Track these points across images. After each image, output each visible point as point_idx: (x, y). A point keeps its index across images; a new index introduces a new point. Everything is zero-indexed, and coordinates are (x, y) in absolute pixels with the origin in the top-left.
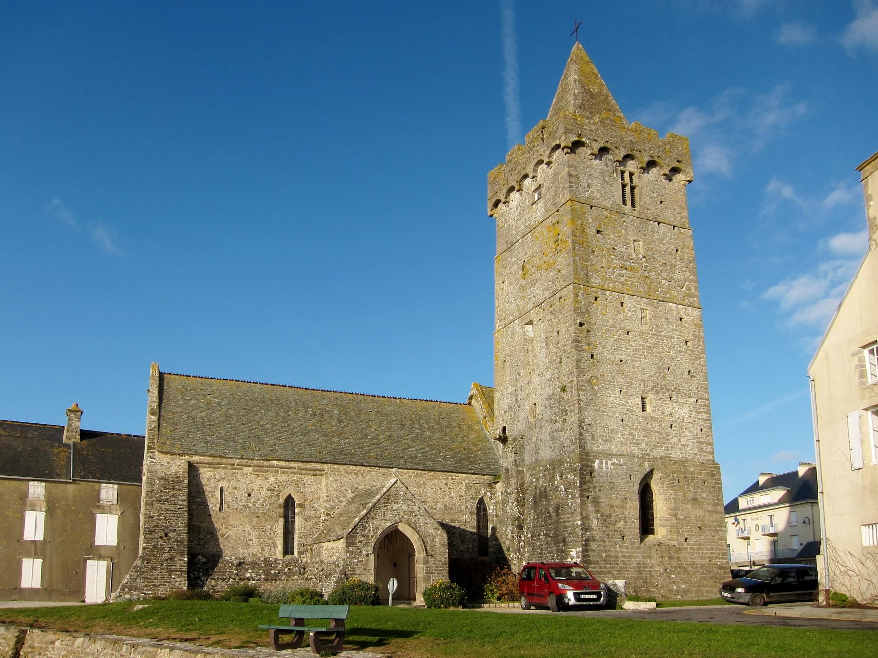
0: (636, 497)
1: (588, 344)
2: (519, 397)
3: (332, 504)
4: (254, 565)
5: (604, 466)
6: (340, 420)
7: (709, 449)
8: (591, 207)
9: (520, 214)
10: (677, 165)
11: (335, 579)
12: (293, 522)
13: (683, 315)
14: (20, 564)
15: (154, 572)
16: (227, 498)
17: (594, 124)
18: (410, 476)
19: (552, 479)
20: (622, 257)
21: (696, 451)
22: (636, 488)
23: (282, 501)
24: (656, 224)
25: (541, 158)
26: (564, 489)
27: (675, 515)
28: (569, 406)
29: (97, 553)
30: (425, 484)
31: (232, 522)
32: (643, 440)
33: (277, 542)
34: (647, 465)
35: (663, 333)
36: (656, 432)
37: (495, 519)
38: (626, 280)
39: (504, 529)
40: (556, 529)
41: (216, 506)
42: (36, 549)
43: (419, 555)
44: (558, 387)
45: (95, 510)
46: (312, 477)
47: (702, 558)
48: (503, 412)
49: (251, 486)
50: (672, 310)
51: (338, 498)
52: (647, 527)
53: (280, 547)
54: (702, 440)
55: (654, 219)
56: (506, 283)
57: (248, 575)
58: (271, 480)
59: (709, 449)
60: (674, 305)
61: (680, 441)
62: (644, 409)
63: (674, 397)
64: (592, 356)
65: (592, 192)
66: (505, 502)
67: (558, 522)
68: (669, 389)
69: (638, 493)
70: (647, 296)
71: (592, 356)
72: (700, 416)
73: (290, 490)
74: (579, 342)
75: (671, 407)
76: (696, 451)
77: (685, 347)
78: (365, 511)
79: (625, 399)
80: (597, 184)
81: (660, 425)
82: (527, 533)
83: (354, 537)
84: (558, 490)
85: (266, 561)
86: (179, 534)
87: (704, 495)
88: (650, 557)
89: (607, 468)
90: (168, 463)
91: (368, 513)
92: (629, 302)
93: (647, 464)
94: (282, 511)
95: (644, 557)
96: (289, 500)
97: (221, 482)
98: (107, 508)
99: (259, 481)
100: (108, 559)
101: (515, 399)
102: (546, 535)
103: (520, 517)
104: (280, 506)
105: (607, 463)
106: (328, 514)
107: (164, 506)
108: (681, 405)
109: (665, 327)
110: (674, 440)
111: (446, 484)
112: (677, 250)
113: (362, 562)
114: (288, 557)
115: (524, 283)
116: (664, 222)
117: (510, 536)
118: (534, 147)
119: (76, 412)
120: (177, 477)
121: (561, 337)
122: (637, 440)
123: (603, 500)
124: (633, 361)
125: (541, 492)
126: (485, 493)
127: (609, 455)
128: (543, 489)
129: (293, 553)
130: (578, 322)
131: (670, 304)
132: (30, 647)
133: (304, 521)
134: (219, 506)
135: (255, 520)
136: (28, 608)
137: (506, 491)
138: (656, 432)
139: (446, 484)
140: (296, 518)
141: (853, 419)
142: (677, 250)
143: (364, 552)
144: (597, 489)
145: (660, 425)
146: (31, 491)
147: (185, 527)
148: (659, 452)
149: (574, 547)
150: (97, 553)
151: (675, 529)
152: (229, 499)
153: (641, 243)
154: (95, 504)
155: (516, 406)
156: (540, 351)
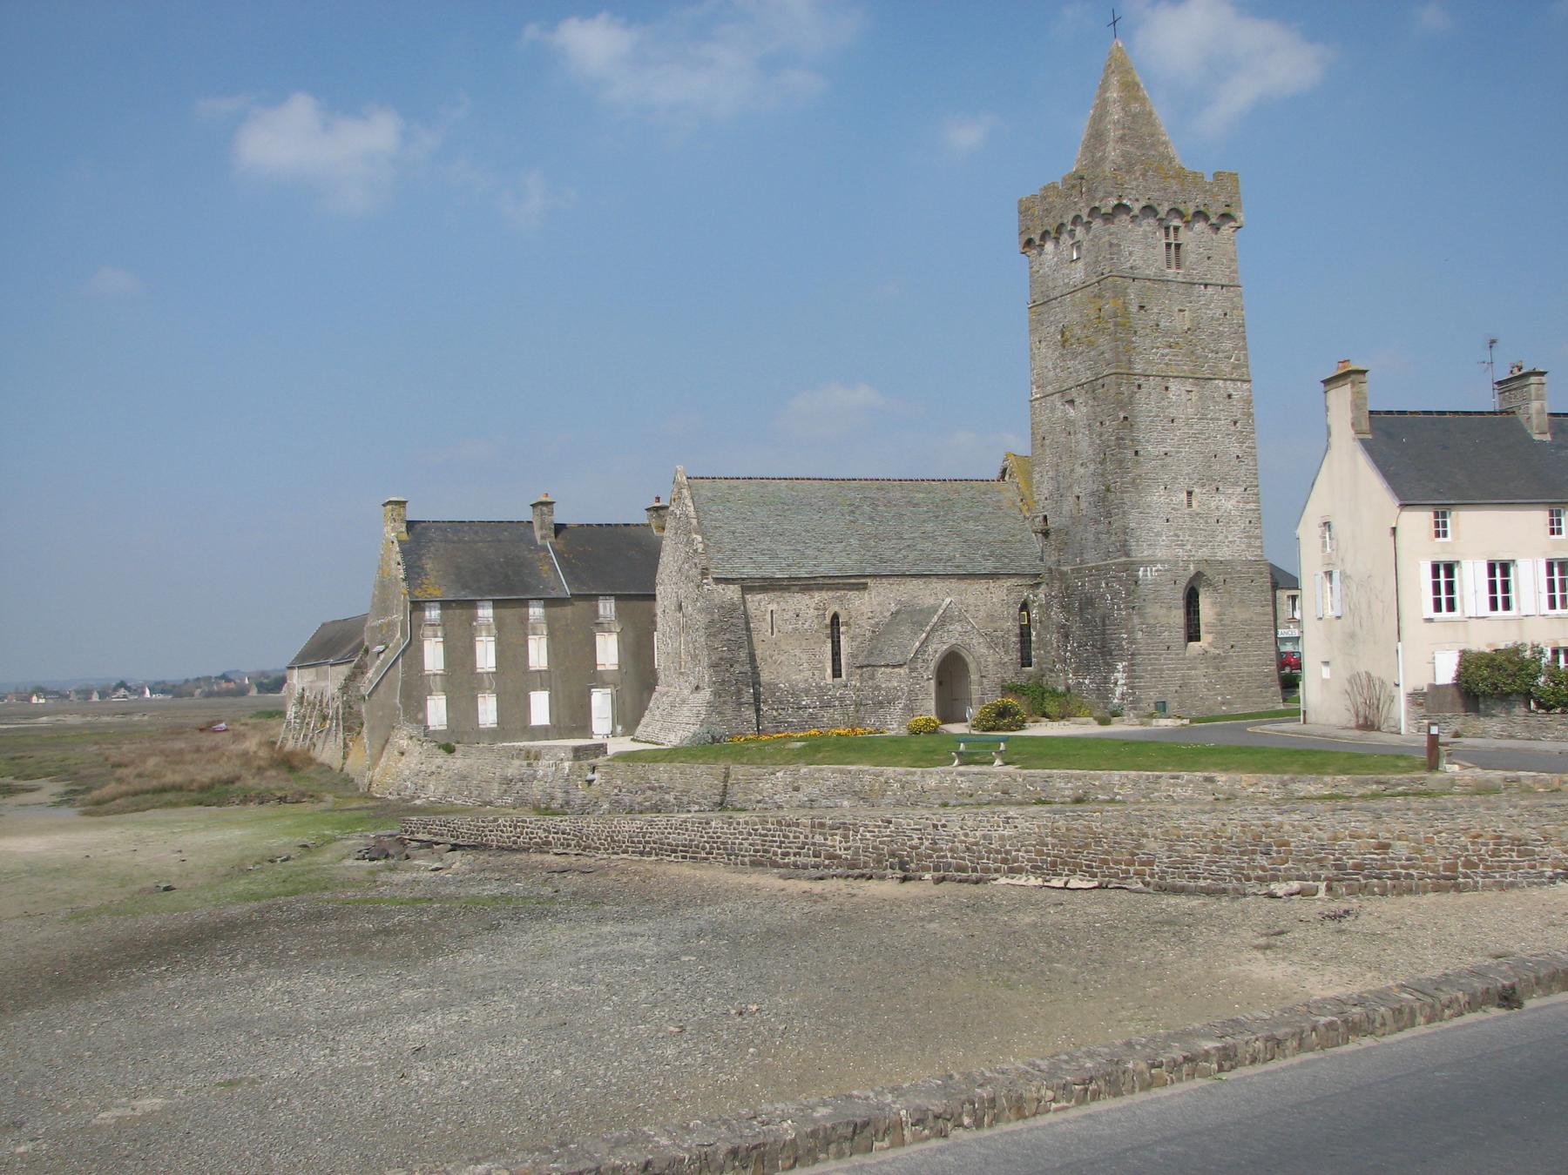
0: (1181, 603)
1: (1132, 440)
2: (1062, 486)
3: (877, 620)
4: (807, 692)
5: (1149, 574)
6: (871, 518)
7: (1258, 543)
8: (1134, 280)
10: (1227, 210)
11: (901, 706)
12: (839, 642)
13: (1231, 391)
14: (528, 698)
17: (1136, 179)
20: (1167, 333)
23: (828, 621)
24: (1202, 286)
25: (1079, 213)
29: (599, 680)
30: (966, 590)
31: (783, 648)
32: (1188, 540)
34: (1192, 568)
35: (1209, 416)
36: (1201, 529)
37: (1038, 624)
38: (1170, 360)
40: (1103, 640)
41: (767, 631)
43: (974, 677)
45: (595, 629)
47: (1248, 665)
48: (1043, 498)
49: (798, 606)
50: (1219, 387)
52: (1193, 634)
53: (829, 671)
54: (1251, 534)
55: (1200, 281)
56: (1044, 344)
59: (1258, 543)
60: (1222, 382)
61: (1227, 537)
62: (1190, 505)
63: (1221, 488)
64: (1136, 453)
65: (1135, 260)
66: (1048, 606)
67: (1103, 633)
68: (1215, 480)
69: (1186, 589)
70: (1192, 375)
71: (1136, 453)
72: (1248, 507)
73: (835, 608)
74: (1123, 439)
77: (1233, 428)
78: (924, 635)
79: (1169, 496)
80: (1138, 250)
81: (1207, 522)
82: (1073, 643)
85: (818, 687)
89: (1152, 575)
90: (723, 590)
91: (927, 637)
92: (1174, 385)
93: (1192, 567)
94: (829, 631)
96: (835, 617)
97: (771, 605)
100: (611, 686)
102: (1092, 645)
103: (1065, 625)
104: (826, 626)
105: (1151, 570)
106: (874, 632)
109: (1212, 408)
111: (988, 589)
112: (1225, 314)
113: (923, 687)
117: (1055, 645)
119: (544, 505)
122: (1182, 541)
124: (1177, 452)
126: (1028, 596)
127: (1154, 563)
128: (1089, 595)
129: (840, 676)
130: (1122, 416)
132: (735, 779)
133: (850, 640)
134: (770, 630)
135: (804, 643)
136: (580, 746)
137: (1050, 595)
138: (1201, 529)
140: (842, 637)
142: (1225, 314)
143: (925, 677)
145: (1207, 522)
147: (746, 657)
148: (1204, 553)
149: (1122, 661)
150: (599, 680)
151: (1220, 635)
152: (780, 622)
154: (594, 625)
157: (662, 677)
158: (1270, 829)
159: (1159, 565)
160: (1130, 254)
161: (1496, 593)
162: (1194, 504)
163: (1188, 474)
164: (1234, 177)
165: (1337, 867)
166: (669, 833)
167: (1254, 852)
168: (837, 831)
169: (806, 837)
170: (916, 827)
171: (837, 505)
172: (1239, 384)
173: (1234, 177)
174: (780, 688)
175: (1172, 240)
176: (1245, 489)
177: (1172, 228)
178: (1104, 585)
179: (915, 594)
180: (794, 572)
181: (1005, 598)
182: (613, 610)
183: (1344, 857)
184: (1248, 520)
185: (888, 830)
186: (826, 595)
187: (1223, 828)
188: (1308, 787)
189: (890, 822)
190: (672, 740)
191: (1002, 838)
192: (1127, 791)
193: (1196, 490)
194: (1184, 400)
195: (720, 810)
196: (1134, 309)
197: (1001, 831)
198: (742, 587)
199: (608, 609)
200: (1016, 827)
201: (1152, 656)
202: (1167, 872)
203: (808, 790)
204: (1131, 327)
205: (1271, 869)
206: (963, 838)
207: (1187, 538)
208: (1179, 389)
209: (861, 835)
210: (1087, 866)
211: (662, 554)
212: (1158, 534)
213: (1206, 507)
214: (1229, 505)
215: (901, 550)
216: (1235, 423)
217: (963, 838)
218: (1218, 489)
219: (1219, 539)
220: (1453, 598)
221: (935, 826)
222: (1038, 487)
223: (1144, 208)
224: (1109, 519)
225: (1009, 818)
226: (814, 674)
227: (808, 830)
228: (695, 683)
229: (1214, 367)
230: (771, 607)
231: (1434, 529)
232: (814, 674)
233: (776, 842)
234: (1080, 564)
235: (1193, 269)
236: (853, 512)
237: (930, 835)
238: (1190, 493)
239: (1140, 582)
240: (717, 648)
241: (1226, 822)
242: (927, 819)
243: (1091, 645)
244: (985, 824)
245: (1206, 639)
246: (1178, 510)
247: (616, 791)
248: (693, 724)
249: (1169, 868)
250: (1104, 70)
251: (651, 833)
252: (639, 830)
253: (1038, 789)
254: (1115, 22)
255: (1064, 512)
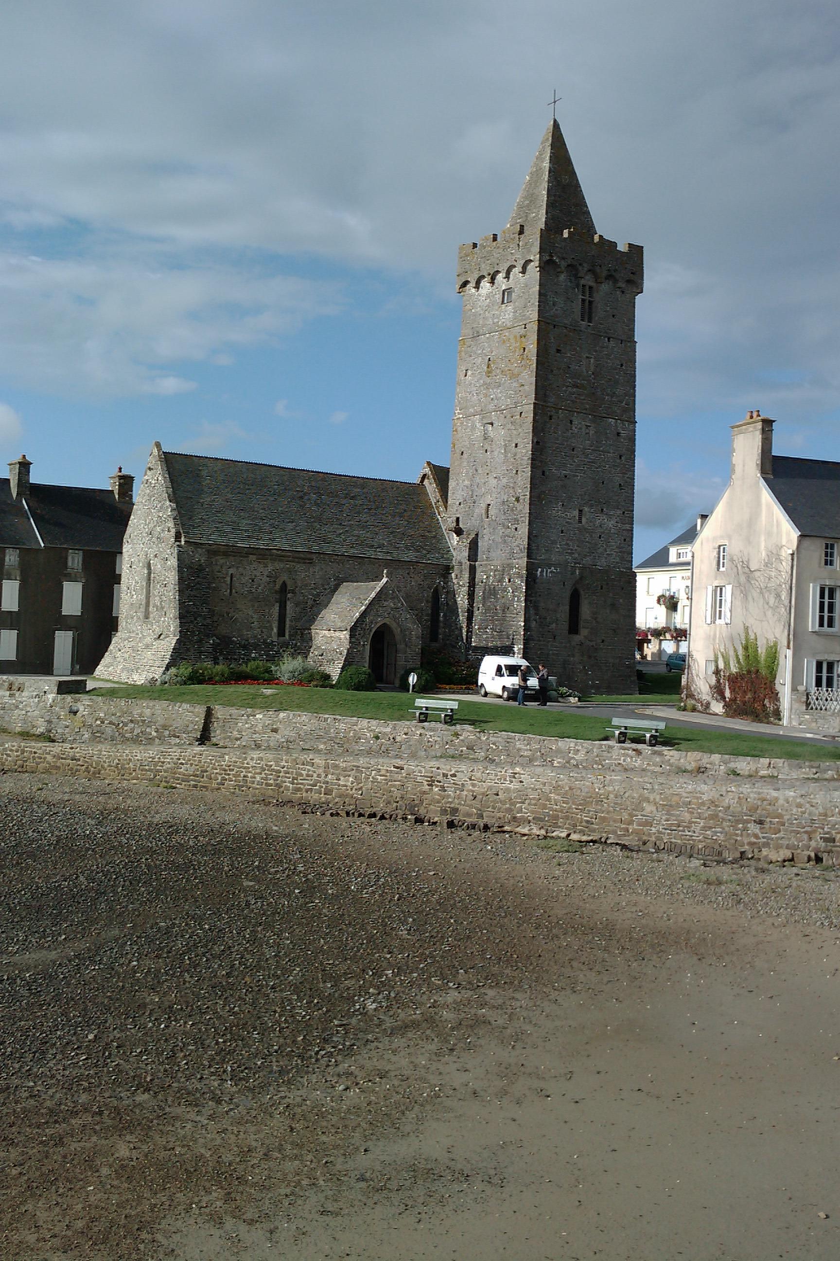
0: (567, 601)
1: (541, 462)
9: (488, 306)
12: (285, 606)
15: (189, 653)
16: (236, 584)
18: (380, 566)
19: (501, 581)
21: (618, 560)
22: (567, 594)
23: (278, 587)
24: (606, 339)
26: (511, 591)
27: (595, 619)
28: (521, 517)
31: (238, 606)
32: (576, 550)
33: (274, 625)
36: (587, 542)
39: (454, 618)
42: (65, 623)
44: (513, 496)
46: (302, 565)
51: (323, 585)
52: (574, 628)
57: (253, 655)
58: (270, 568)
60: (614, 420)
67: (504, 619)
73: (284, 577)
75: (602, 519)
76: (618, 560)
77: (618, 461)
83: (356, 629)
84: (506, 591)
86: (205, 619)
87: (621, 601)
88: (573, 656)
90: (193, 552)
95: (569, 656)
96: (284, 584)
98: (73, 575)
99: (261, 568)
101: (470, 493)
104: (276, 592)
105: (547, 571)
106: (315, 601)
107: (192, 593)
108: (610, 517)
110: (600, 550)
111: (408, 574)
113: (359, 651)
114: (282, 639)
115: (488, 380)
116: (613, 336)
118: (509, 247)
120: (200, 565)
121: (518, 450)
122: (572, 550)
123: (542, 605)
125: (490, 590)
126: (439, 583)
131: (611, 420)
134: (229, 591)
135: (256, 605)
139: (408, 574)
140: (288, 603)
141: (710, 589)
142: (622, 365)
143: (362, 643)
144: (538, 594)
145: (591, 536)
146: (7, 559)
148: (588, 561)
153: (592, 360)
155: (471, 500)
156: (498, 455)
157: (122, 624)
158: (765, 803)
159: (553, 568)
160: (554, 305)
161: (829, 616)
162: (584, 520)
163: (581, 495)
164: (641, 248)
165: (826, 840)
166: (182, 764)
167: (748, 822)
168: (349, 773)
169: (319, 776)
170: (426, 774)
171: (289, 490)
172: (627, 423)
173: (641, 248)
174: (233, 641)
175: (587, 298)
176: (624, 513)
177: (587, 287)
178: (507, 580)
179: (351, 573)
180: (253, 543)
181: (422, 583)
182: (81, 562)
183: (833, 832)
184: (623, 538)
185: (400, 775)
186: (278, 565)
187: (721, 798)
188: (743, 765)
189: (402, 769)
190: (139, 679)
191: (508, 790)
192: (580, 756)
193: (586, 509)
194: (584, 433)
195: (199, 744)
196: (553, 351)
197: (507, 784)
198: (208, 551)
199: (76, 561)
200: (521, 782)
201: (542, 643)
202: (664, 834)
203: (286, 732)
204: (549, 366)
205: (764, 838)
206: (471, 788)
207: (576, 548)
208: (580, 423)
209: (373, 778)
210: (587, 822)
211: (132, 517)
212: (554, 542)
213: (591, 524)
214: (611, 524)
215: (340, 534)
216: (620, 457)
217: (471, 788)
218: (602, 510)
219: (600, 550)
220: (832, 616)
221: (445, 775)
222: (453, 493)
223: (568, 266)
224: (516, 526)
225: (516, 773)
226: (262, 632)
227: (321, 771)
228: (158, 631)
229: (609, 408)
230: (231, 571)
231: (823, 558)
232: (262, 632)
233: (289, 778)
234: (487, 560)
235: (601, 324)
236: (301, 497)
237: (440, 782)
238: (581, 511)
239: (537, 581)
240: (185, 602)
241: (724, 794)
242: (438, 768)
243: (491, 629)
244: (493, 777)
245: (584, 632)
246: (571, 523)
247: (98, 722)
248: (159, 667)
249: (666, 829)
250: (542, 144)
251: (163, 762)
252: (150, 760)
253: (500, 748)
254: (555, 102)
255: (475, 516)
